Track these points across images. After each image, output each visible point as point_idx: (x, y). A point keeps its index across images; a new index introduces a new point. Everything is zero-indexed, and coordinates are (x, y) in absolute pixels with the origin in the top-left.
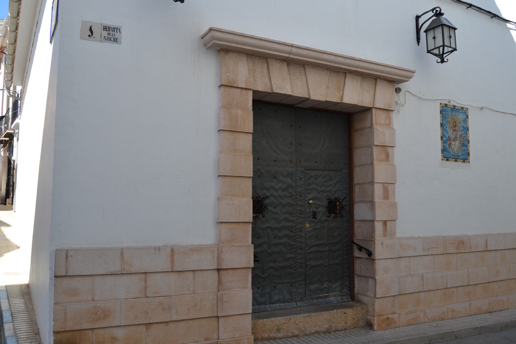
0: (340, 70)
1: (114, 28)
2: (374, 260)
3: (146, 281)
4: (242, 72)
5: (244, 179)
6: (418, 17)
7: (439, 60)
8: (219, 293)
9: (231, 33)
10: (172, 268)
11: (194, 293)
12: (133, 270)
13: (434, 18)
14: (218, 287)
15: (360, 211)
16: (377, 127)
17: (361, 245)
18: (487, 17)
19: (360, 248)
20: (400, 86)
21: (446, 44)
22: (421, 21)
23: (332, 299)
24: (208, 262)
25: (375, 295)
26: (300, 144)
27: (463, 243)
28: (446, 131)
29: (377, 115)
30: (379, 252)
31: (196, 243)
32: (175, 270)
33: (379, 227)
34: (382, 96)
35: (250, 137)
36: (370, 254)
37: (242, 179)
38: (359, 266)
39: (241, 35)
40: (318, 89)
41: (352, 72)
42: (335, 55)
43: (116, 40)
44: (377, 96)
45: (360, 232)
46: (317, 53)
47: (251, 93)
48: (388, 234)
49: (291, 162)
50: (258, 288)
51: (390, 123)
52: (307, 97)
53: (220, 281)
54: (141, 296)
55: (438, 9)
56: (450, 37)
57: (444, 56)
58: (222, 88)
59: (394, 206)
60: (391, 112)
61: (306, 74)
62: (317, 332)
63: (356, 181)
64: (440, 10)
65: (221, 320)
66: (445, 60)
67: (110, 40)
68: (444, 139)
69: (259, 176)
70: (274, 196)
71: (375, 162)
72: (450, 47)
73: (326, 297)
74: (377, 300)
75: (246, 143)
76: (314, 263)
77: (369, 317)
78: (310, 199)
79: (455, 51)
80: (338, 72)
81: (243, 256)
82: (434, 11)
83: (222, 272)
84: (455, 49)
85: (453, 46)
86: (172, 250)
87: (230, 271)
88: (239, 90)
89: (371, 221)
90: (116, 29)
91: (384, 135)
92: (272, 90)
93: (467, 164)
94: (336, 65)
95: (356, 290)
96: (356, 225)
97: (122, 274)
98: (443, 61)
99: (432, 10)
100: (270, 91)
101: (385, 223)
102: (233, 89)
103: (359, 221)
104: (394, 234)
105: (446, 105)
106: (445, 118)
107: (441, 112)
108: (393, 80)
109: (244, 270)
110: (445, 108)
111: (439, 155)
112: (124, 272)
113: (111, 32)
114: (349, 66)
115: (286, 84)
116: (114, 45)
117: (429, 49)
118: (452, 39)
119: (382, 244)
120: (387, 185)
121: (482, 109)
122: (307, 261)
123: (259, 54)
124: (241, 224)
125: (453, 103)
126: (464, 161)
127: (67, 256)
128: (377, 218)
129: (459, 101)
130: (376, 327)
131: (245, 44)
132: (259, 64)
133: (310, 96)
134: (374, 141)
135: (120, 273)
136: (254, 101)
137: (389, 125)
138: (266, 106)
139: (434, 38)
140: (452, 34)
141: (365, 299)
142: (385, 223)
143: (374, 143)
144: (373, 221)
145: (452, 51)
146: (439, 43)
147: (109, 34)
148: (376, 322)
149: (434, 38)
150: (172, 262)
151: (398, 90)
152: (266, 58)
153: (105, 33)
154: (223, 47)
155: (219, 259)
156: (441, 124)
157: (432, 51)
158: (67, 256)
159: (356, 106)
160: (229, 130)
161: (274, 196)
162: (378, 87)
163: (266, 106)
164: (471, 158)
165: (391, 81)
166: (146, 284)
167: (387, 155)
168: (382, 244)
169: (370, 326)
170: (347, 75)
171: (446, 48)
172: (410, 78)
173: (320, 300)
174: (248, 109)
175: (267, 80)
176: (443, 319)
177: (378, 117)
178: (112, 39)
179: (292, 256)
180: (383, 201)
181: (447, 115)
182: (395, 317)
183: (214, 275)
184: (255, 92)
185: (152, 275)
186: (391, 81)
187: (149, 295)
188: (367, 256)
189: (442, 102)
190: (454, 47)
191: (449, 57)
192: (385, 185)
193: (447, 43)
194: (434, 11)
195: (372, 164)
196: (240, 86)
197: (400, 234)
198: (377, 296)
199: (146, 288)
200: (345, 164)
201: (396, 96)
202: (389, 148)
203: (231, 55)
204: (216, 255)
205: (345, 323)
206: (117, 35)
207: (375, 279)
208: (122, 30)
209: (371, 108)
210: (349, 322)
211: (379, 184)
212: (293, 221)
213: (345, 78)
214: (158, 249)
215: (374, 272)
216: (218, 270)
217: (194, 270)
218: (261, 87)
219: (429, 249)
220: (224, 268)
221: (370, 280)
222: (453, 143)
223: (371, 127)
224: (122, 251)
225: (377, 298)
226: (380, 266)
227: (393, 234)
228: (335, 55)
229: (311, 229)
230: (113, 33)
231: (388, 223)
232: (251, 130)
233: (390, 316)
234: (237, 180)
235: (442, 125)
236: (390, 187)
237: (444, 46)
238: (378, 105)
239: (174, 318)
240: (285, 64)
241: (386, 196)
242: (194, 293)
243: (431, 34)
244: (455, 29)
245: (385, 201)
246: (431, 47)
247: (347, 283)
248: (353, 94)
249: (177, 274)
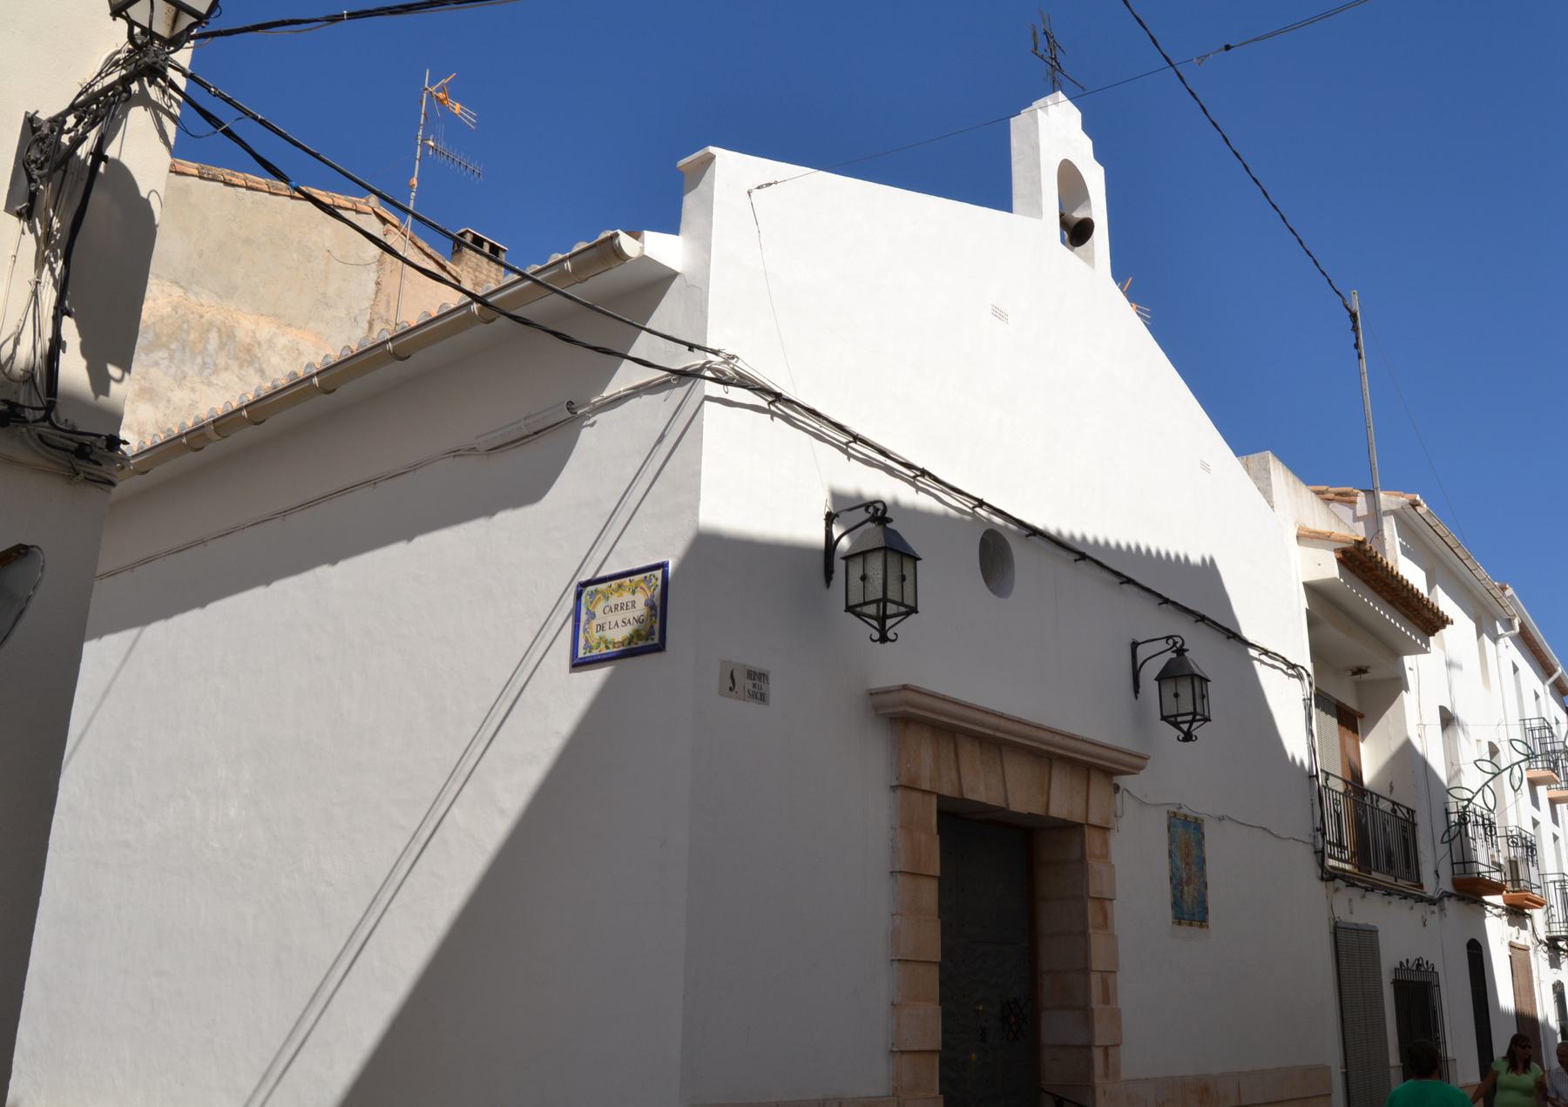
4: (926, 759)
6: (1135, 645)
7: (876, 635)
13: (870, 525)
15: (1055, 1027)
18: (1220, 636)
21: (890, 595)
22: (1142, 653)
33: (1098, 1055)
41: (1061, 758)
47: (934, 800)
55: (880, 506)
56: (903, 578)
57: (889, 623)
58: (899, 792)
59: (1116, 1016)
66: (890, 635)
71: (1091, 930)
72: (901, 604)
82: (871, 510)
84: (913, 610)
85: (909, 601)
98: (884, 639)
99: (1168, 638)
101: (1106, 1048)
108: (1100, 769)
114: (990, 727)
115: (984, 785)
117: (852, 603)
118: (908, 584)
128: (1097, 1043)
129: (1195, 806)
136: (940, 812)
140: (908, 571)
145: (907, 614)
146: (875, 591)
149: (1176, 695)
171: (889, 605)
177: (1093, 841)
191: (1199, 731)
193: (893, 594)
194: (871, 510)
195: (1084, 934)
197: (1126, 1073)
209: (1081, 825)
218: (947, 790)
223: (1082, 860)
231: (1111, 1051)
232: (937, 871)
237: (885, 600)
241: (1107, 998)
243: (856, 570)
246: (855, 599)
248: (1063, 801)
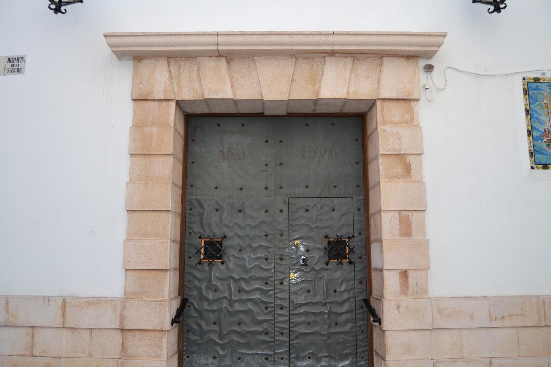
1: (18, 59)
3: (33, 337)
4: (159, 79)
5: (160, 214)
9: (130, 36)
10: (63, 324)
11: (90, 357)
12: (19, 322)
16: (385, 128)
24: (108, 320)
26: (281, 164)
28: (539, 120)
29: (385, 111)
31: (98, 295)
32: (67, 325)
34: (391, 81)
37: (156, 213)
39: (143, 35)
40: (272, 86)
42: (289, 34)
43: (19, 71)
46: (259, 37)
47: (173, 105)
48: (410, 290)
49: (266, 188)
50: (214, 358)
51: (412, 119)
53: (123, 346)
54: (26, 354)
59: (423, 247)
60: (413, 104)
63: (371, 212)
67: (14, 72)
68: (535, 134)
69: (217, 210)
70: (238, 236)
76: (302, 329)
78: (297, 239)
80: (312, 58)
81: (160, 311)
86: (64, 302)
87: (137, 333)
88: (156, 103)
90: (21, 59)
91: (400, 138)
94: (295, 48)
97: (6, 326)
102: (149, 103)
104: (425, 290)
106: (536, 101)
107: (526, 92)
108: (418, 54)
109: (156, 333)
110: (534, 85)
111: (526, 160)
112: (8, 325)
113: (15, 63)
114: (394, 45)
115: (220, 86)
116: (17, 76)
119: (398, 307)
120: (407, 214)
122: (291, 326)
123: (179, 55)
124: (153, 272)
131: (152, 45)
132: (187, 66)
135: (4, 325)
137: (410, 121)
142: (404, 274)
144: (381, 270)
147: (13, 66)
150: (64, 316)
151: (429, 68)
152: (168, 58)
153: (9, 66)
154: (137, 54)
155: (122, 318)
156: (526, 110)
160: (142, 153)
161: (238, 236)
165: (411, 57)
166: (33, 340)
167: (408, 169)
168: (398, 307)
174: (169, 124)
175: (196, 85)
178: (16, 70)
179: (268, 318)
180: (401, 238)
181: (540, 96)
183: (117, 337)
185: (40, 330)
187: (36, 353)
189: (525, 75)
192: (403, 213)
196: (156, 98)
199: (33, 345)
200: (358, 186)
201: (424, 78)
202: (411, 157)
203: (146, 62)
204: (118, 311)
206: (21, 65)
208: (27, 60)
211: (392, 214)
212: (269, 270)
214: (48, 299)
216: (122, 330)
217: (91, 328)
218: (186, 95)
219: (503, 318)
224: (7, 300)
227: (422, 292)
228: (289, 34)
229: (299, 280)
230: (17, 64)
231: (412, 275)
234: (149, 215)
235: (528, 112)
236: (414, 218)
238: (385, 94)
240: (223, 63)
242: (90, 357)
245: (406, 239)
247: (363, 363)
248: (335, 86)
249: (70, 331)
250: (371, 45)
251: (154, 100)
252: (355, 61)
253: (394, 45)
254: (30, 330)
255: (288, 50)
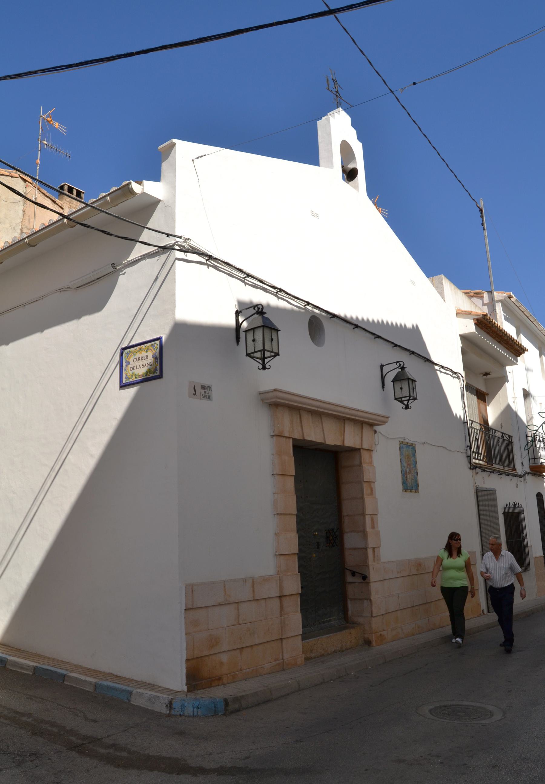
0: (343, 418)
2: (368, 583)
3: (238, 610)
7: (261, 367)
8: (282, 617)
10: (254, 597)
14: (281, 612)
15: (351, 540)
17: (354, 570)
19: (354, 574)
20: (375, 428)
21: (266, 348)
23: (333, 622)
25: (372, 614)
27: (420, 565)
30: (373, 576)
32: (256, 599)
33: (370, 552)
35: (292, 479)
36: (365, 578)
38: (351, 591)
41: (349, 419)
44: (364, 438)
45: (351, 560)
52: (323, 442)
53: (282, 607)
56: (272, 340)
58: (275, 438)
59: (378, 534)
61: (322, 422)
62: (335, 651)
64: (404, 365)
65: (284, 641)
66: (267, 366)
71: (365, 496)
72: (272, 352)
73: (329, 621)
74: (373, 619)
75: (290, 483)
77: (366, 636)
78: (315, 531)
79: (278, 356)
81: (293, 585)
83: (283, 599)
84: (277, 354)
85: (275, 350)
88: (284, 439)
89: (363, 548)
92: (304, 437)
93: (417, 493)
94: (299, 405)
95: (350, 613)
96: (347, 553)
100: (301, 438)
101: (374, 549)
103: (350, 549)
105: (402, 442)
108: (366, 423)
111: (400, 487)
114: (374, 420)
117: (249, 352)
118: (275, 342)
121: (424, 444)
125: (407, 441)
126: (416, 492)
127: (192, 591)
129: (411, 438)
130: (374, 643)
131: (361, 417)
133: (325, 441)
134: (363, 477)
136: (294, 446)
138: (304, 451)
139: (401, 388)
141: (361, 620)
143: (363, 479)
144: (366, 549)
145: (275, 356)
146: (259, 347)
147: (205, 392)
148: (373, 638)
149: (401, 388)
150: (253, 591)
155: (281, 588)
157: (252, 355)
158: (192, 591)
159: (352, 447)
162: (346, 426)
163: (304, 451)
164: (420, 488)
165: (371, 425)
169: (368, 643)
170: (346, 421)
172: (385, 422)
173: (326, 624)
176: (413, 635)
177: (365, 456)
182: (384, 633)
184: (294, 440)
186: (371, 425)
188: (361, 580)
190: (277, 352)
193: (268, 347)
195: (362, 498)
198: (374, 615)
205: (351, 642)
207: (371, 600)
208: (213, 388)
209: (360, 449)
210: (353, 641)
213: (344, 424)
215: (369, 594)
216: (280, 597)
218: (297, 436)
220: (285, 594)
221: (365, 601)
222: (408, 476)
223: (360, 465)
225: (373, 617)
226: (374, 587)
233: (382, 633)
238: (364, 447)
239: (257, 642)
243: (250, 337)
244: (415, 381)
248: (350, 438)
250: (376, 421)
251: (302, 430)
252: (259, 538)
253: (374, 420)
254: (237, 605)
255: (308, 408)
